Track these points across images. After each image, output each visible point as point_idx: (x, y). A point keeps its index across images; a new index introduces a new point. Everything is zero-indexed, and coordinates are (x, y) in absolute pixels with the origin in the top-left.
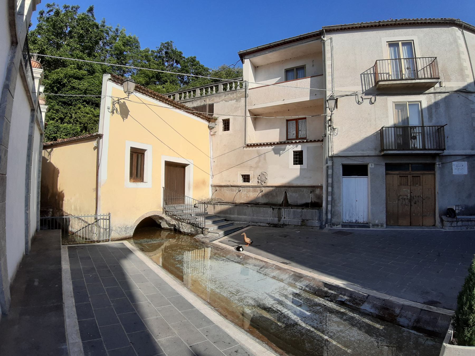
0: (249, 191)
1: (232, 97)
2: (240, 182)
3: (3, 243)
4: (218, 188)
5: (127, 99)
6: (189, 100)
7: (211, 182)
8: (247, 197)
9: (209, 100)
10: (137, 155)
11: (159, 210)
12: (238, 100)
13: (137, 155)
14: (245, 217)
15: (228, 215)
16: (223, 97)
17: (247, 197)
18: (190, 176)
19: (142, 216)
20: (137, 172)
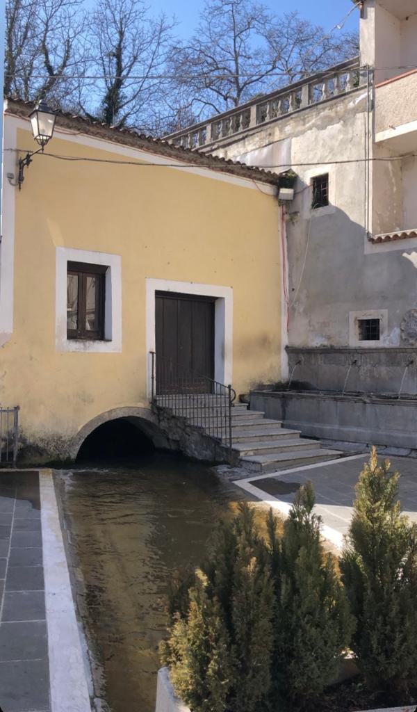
0: (379, 363)
1: (333, 114)
2: (353, 339)
3: (79, 571)
4: (302, 358)
5: (41, 151)
6: (236, 138)
7: (285, 341)
8: (372, 377)
9: (281, 131)
10: (89, 279)
11: (141, 405)
12: (346, 119)
13: (89, 279)
14: (355, 429)
15: (316, 426)
16: (314, 120)
17: (372, 377)
18: (229, 328)
19: (99, 417)
20: (89, 322)
